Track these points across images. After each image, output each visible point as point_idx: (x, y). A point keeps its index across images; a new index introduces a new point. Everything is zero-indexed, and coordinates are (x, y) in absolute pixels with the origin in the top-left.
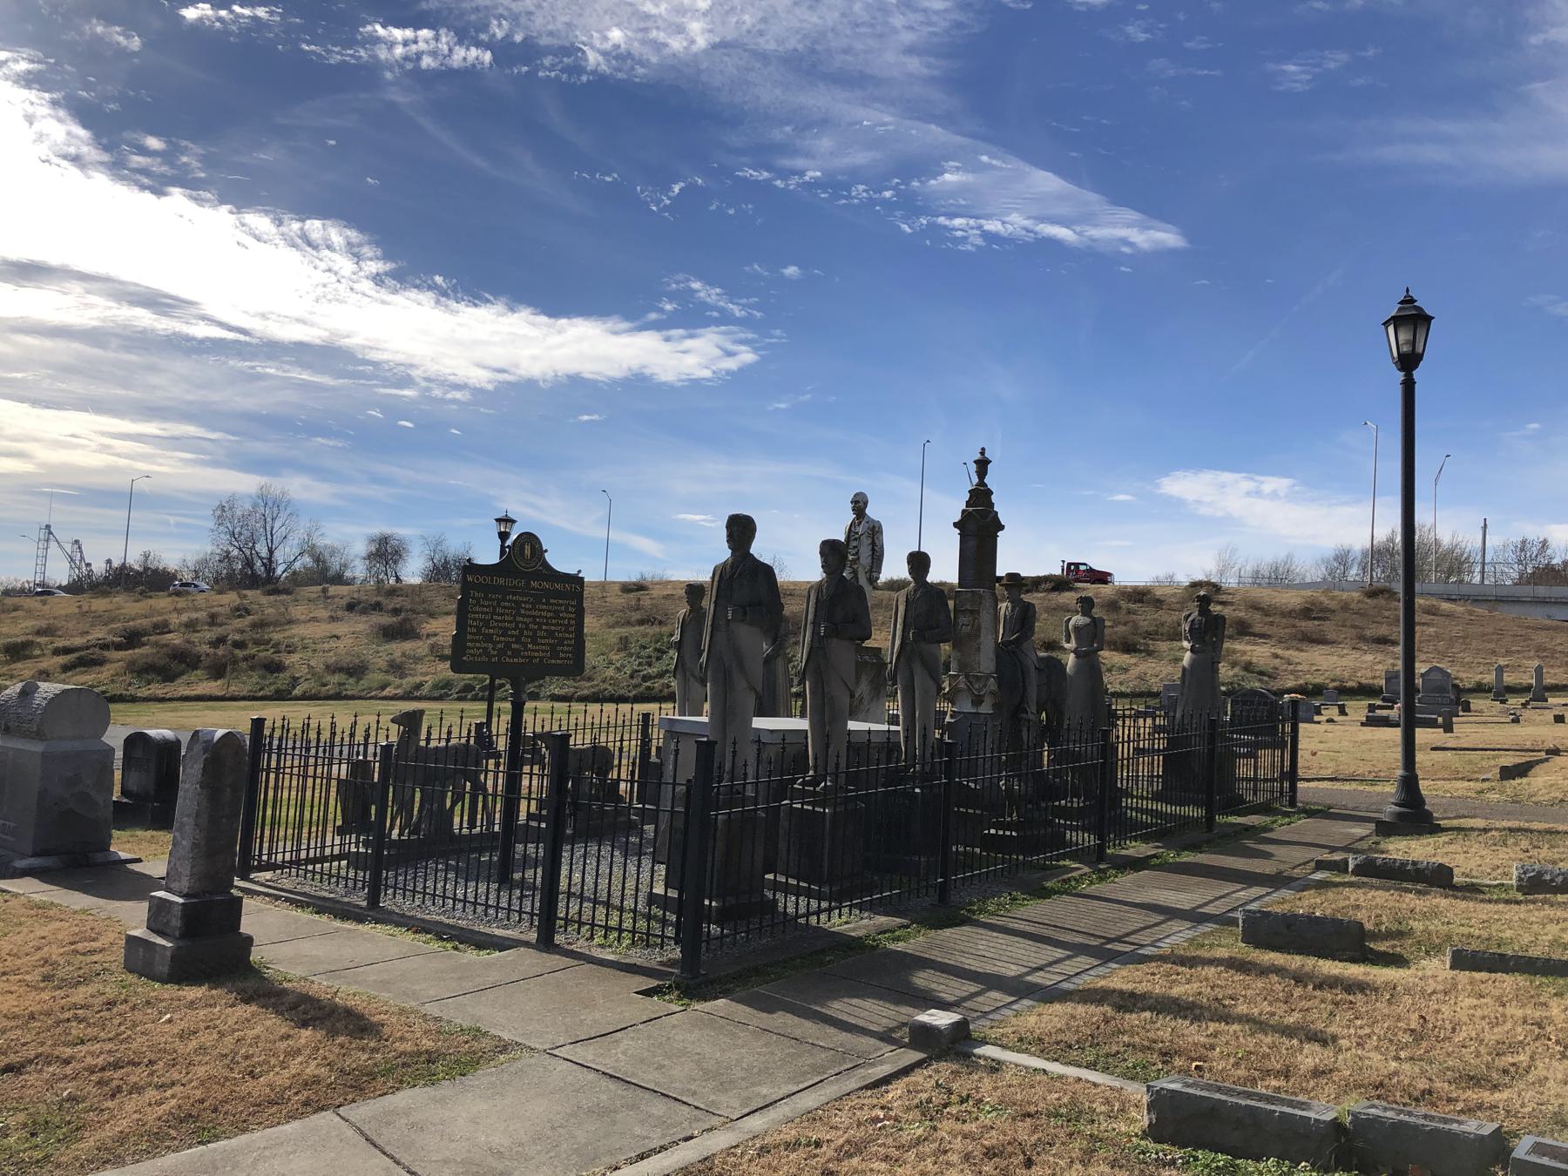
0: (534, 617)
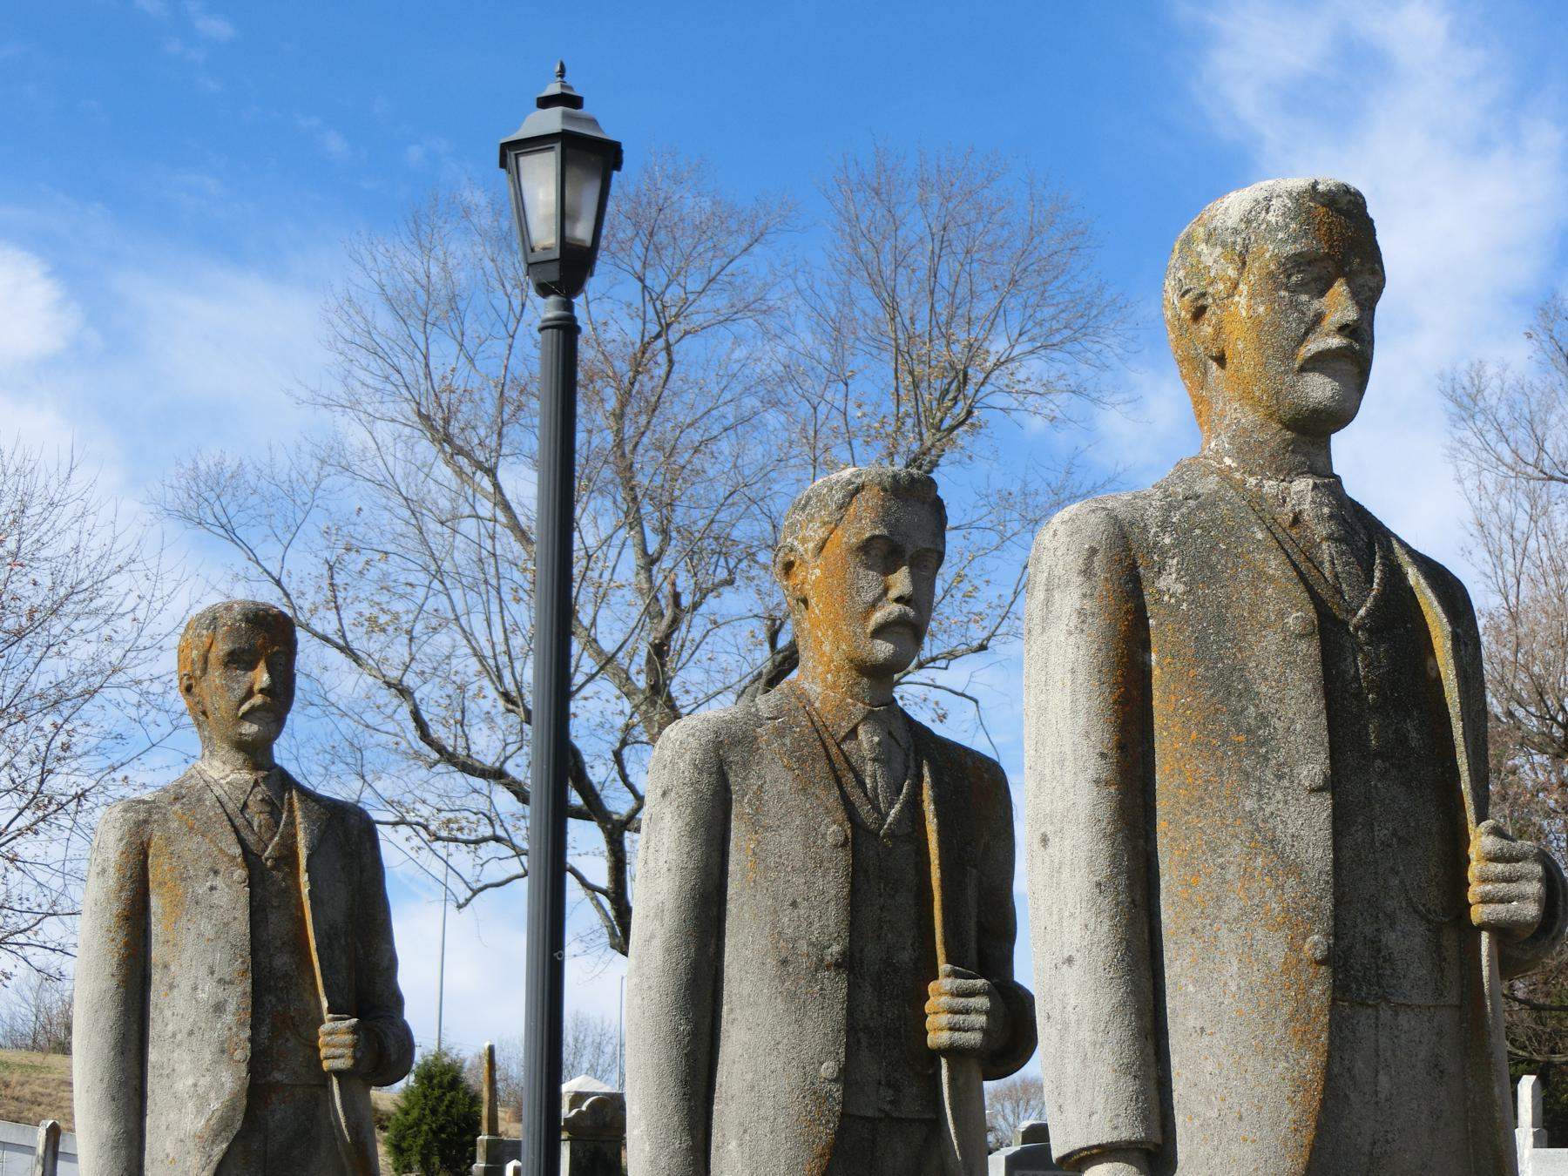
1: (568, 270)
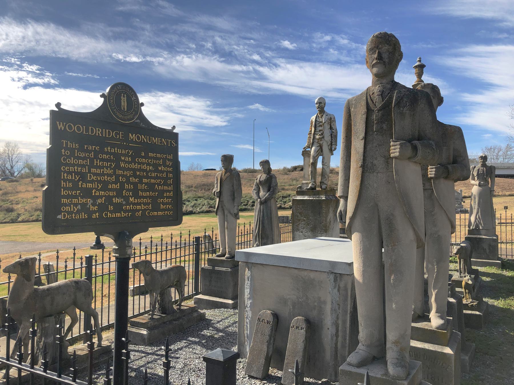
0: (134, 170)
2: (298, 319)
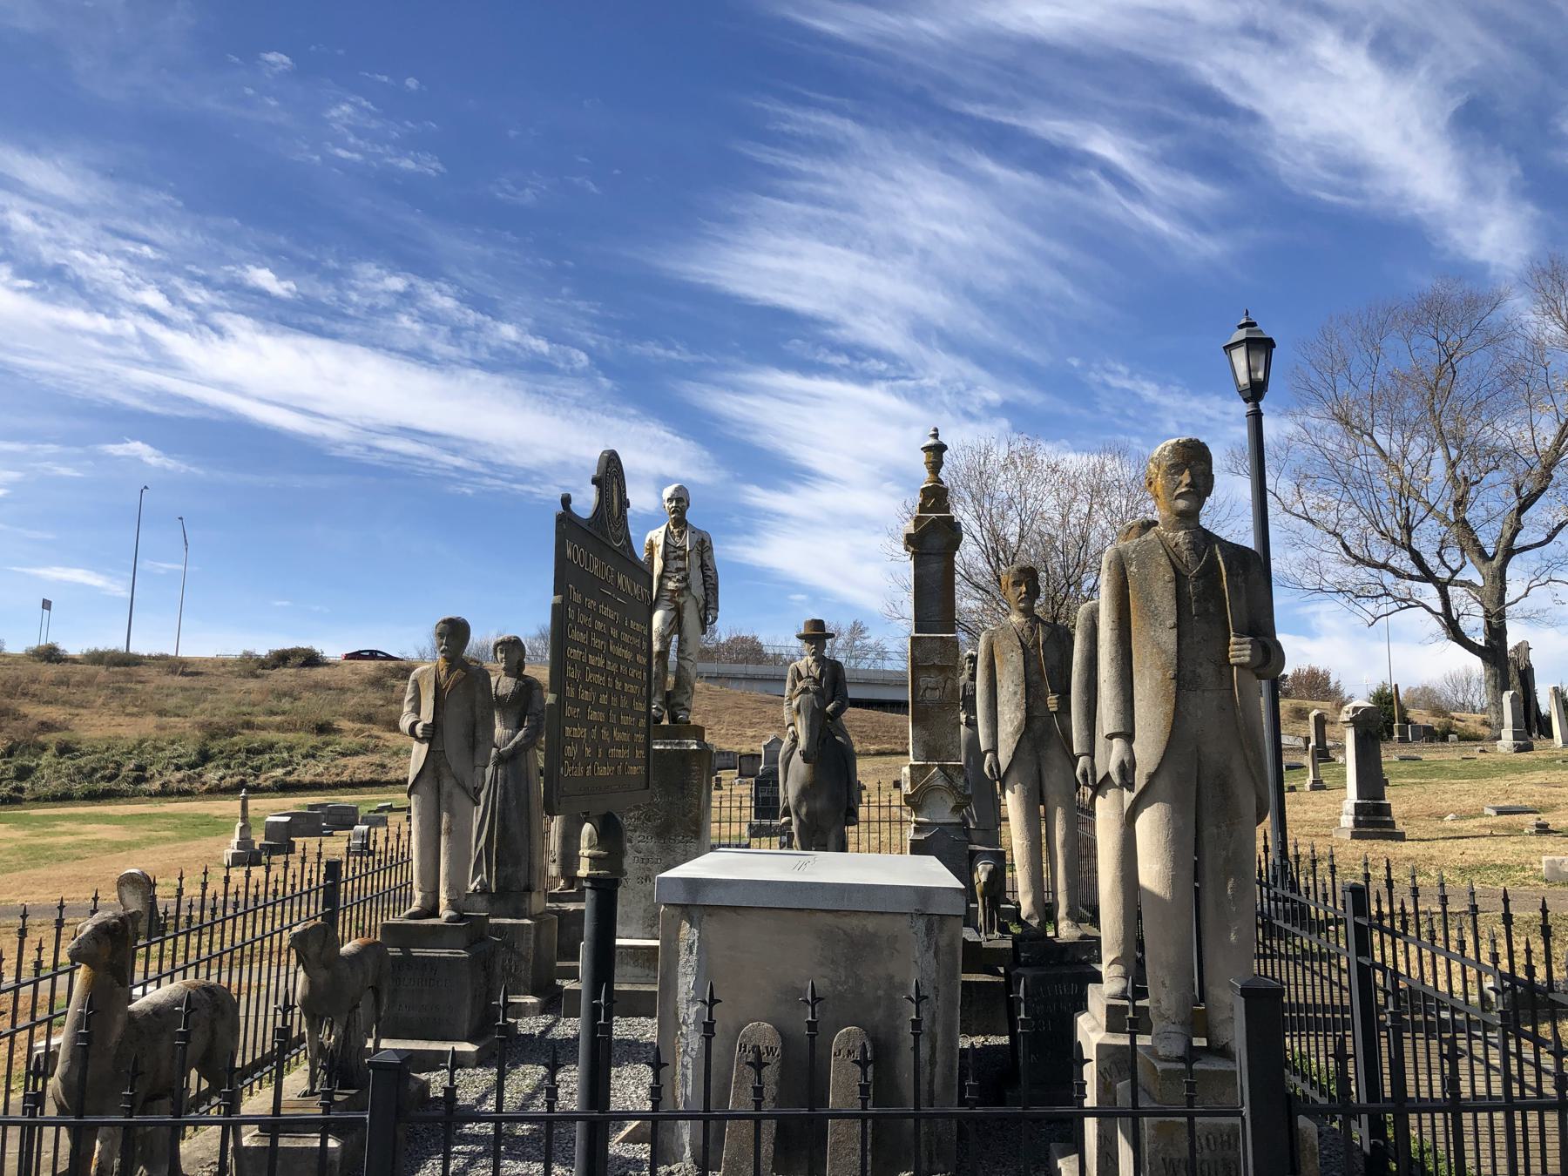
1: (1255, 392)
2: (848, 1033)
